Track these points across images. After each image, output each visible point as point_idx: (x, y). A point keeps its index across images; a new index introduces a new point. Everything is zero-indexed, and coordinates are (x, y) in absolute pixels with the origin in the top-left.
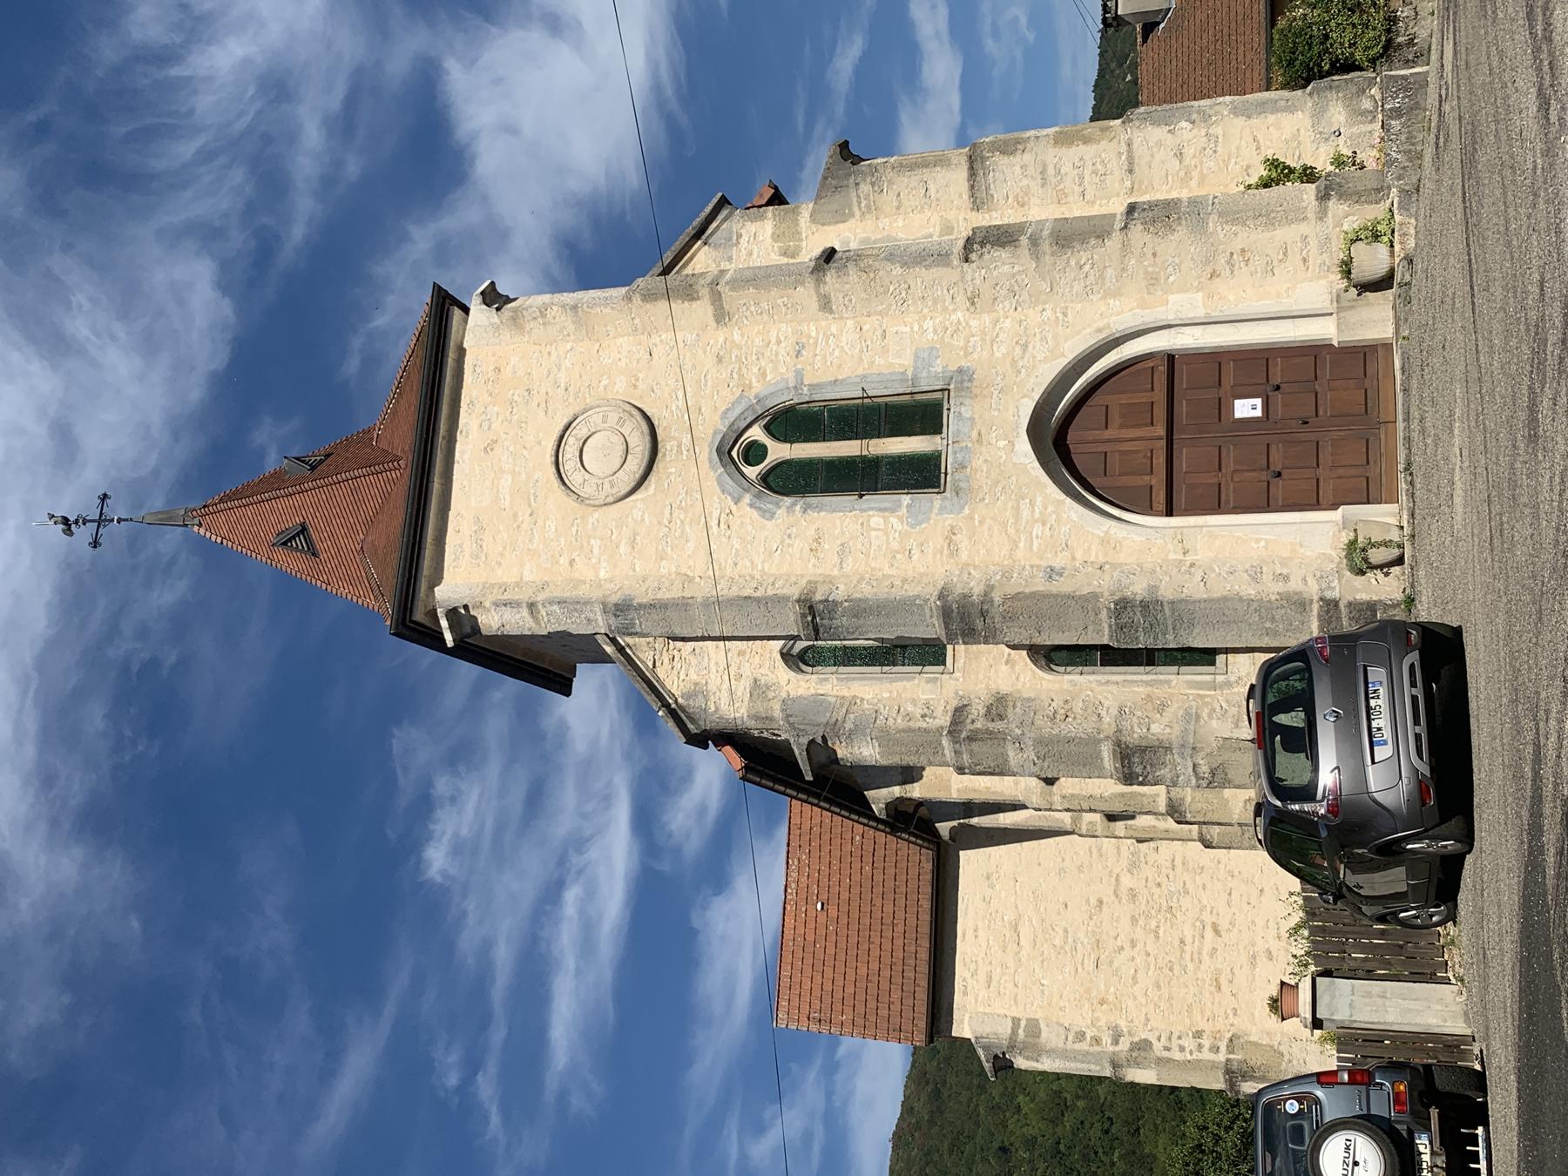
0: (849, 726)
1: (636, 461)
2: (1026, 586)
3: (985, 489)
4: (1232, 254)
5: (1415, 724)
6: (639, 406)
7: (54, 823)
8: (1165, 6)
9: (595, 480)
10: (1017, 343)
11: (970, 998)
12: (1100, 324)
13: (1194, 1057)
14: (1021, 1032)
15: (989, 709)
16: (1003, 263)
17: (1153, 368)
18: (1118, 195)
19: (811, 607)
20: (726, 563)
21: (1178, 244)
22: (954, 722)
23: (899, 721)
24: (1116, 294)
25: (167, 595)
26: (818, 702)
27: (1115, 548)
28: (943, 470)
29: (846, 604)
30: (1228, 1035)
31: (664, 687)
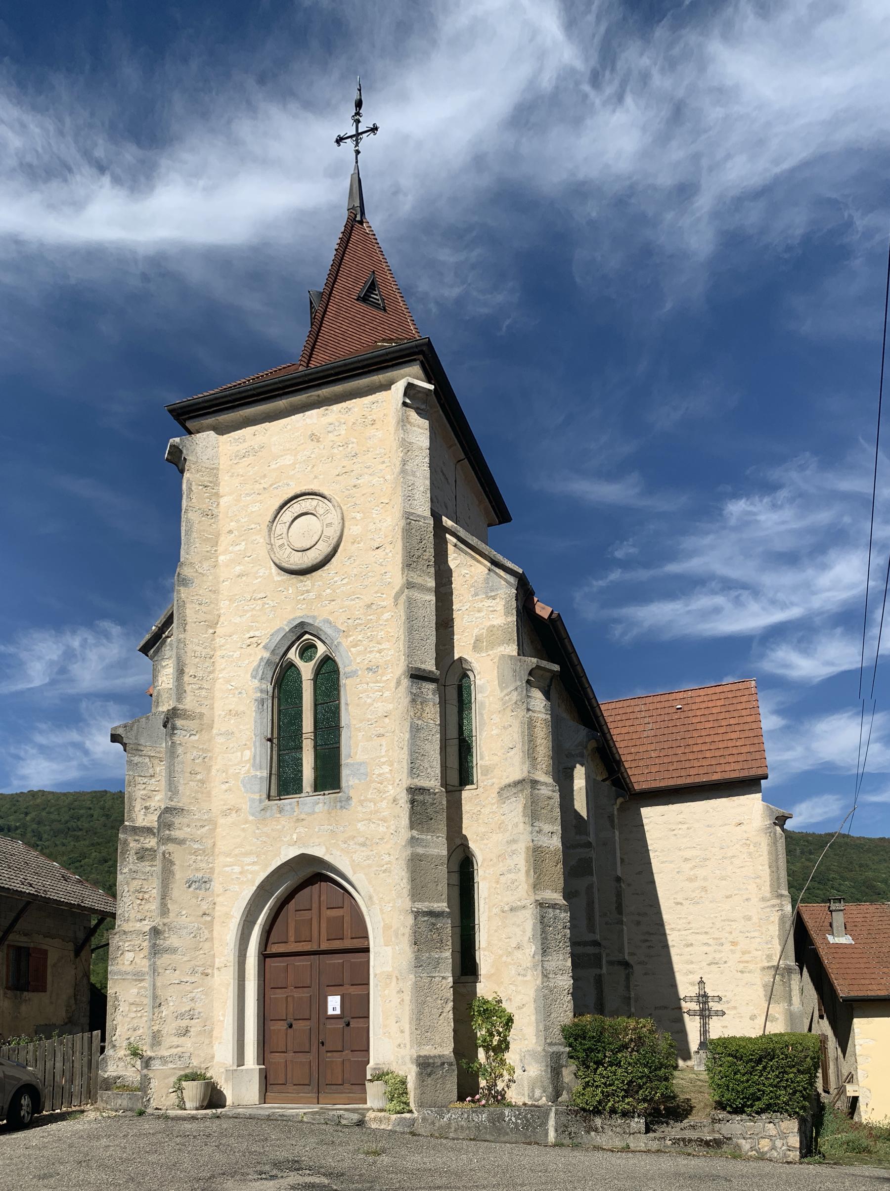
0: (136, 759)
1: (296, 560)
3: (265, 830)
9: (285, 531)
10: (367, 838)
12: (375, 899)
23: (142, 792)
27: (223, 922)
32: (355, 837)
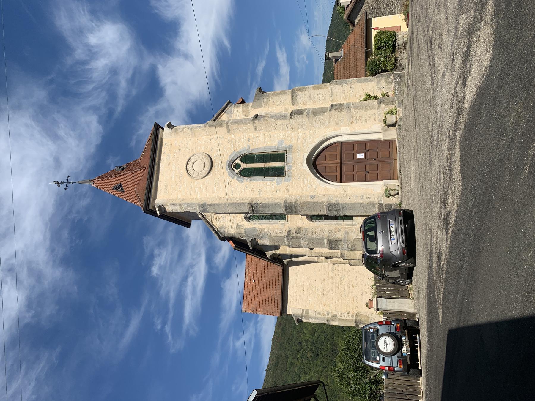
0: (261, 235)
2: (306, 200)
4: (357, 117)
5: (401, 225)
6: (208, 154)
7: (54, 261)
8: (340, 55)
11: (292, 304)
12: (324, 135)
13: (347, 318)
14: (304, 312)
15: (296, 231)
16: (300, 119)
17: (337, 146)
18: (329, 102)
19: (252, 205)
20: (230, 194)
21: (343, 115)
22: (288, 234)
24: (328, 127)
25: (85, 202)
26: (254, 229)
28: (285, 171)
29: (261, 204)
30: (356, 313)
31: (214, 226)
32: (302, 143)
